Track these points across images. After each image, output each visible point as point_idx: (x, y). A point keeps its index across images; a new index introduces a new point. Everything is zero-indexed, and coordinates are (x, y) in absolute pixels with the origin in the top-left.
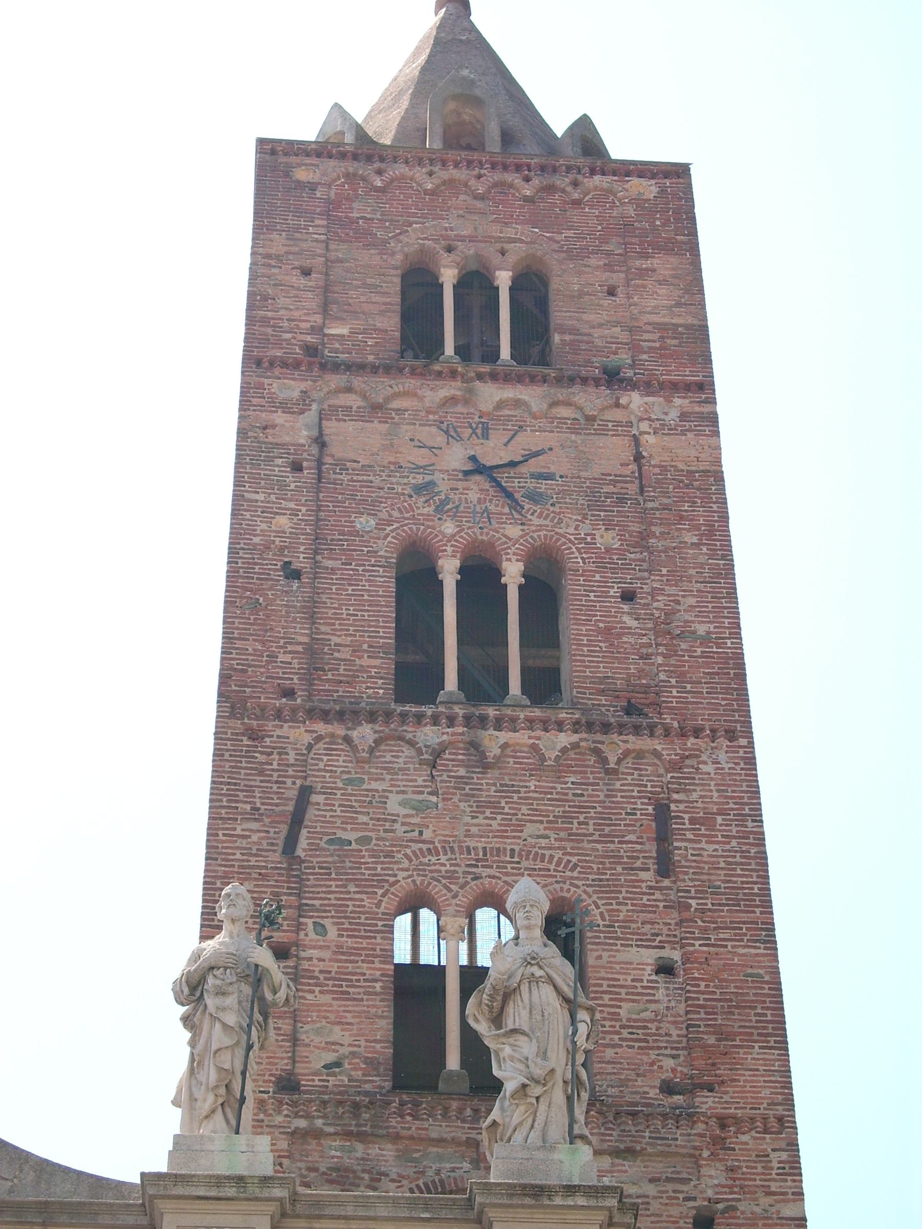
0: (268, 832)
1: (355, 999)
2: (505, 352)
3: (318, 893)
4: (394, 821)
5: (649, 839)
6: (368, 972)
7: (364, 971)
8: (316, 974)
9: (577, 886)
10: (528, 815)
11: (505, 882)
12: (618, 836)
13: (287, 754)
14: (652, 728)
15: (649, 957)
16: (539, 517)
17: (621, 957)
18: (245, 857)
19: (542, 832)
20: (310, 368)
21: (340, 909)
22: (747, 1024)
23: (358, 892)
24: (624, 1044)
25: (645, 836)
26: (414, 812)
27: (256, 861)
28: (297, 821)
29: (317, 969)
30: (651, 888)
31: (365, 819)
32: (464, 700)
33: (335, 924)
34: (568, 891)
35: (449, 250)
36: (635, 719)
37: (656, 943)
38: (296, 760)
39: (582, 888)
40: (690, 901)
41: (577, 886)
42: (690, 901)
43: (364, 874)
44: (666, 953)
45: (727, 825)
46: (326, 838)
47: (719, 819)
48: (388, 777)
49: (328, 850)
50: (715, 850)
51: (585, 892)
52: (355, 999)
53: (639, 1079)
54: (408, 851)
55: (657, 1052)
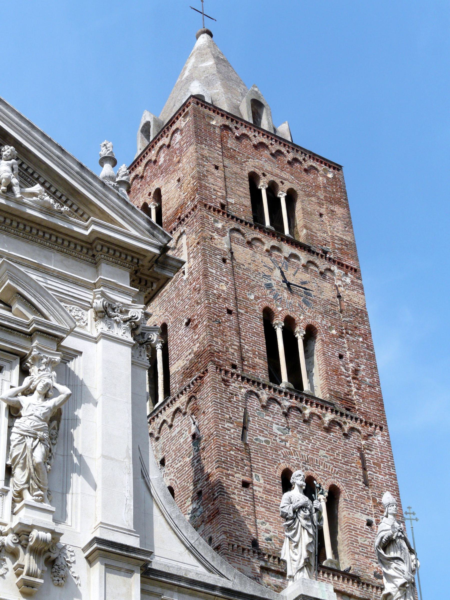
0: (236, 430)
2: (268, 223)
4: (276, 436)
5: (360, 467)
6: (275, 501)
7: (274, 500)
8: (259, 498)
12: (350, 463)
13: (238, 396)
15: (365, 518)
16: (308, 312)
18: (230, 439)
19: (325, 455)
20: (255, 228)
23: (268, 465)
24: (361, 553)
25: (358, 465)
28: (245, 428)
29: (259, 496)
32: (293, 388)
33: (263, 477)
35: (264, 175)
36: (348, 413)
37: (366, 513)
38: (242, 399)
41: (339, 481)
43: (269, 457)
44: (370, 518)
48: (272, 416)
49: (255, 443)
50: (382, 478)
53: (368, 570)
54: (283, 451)
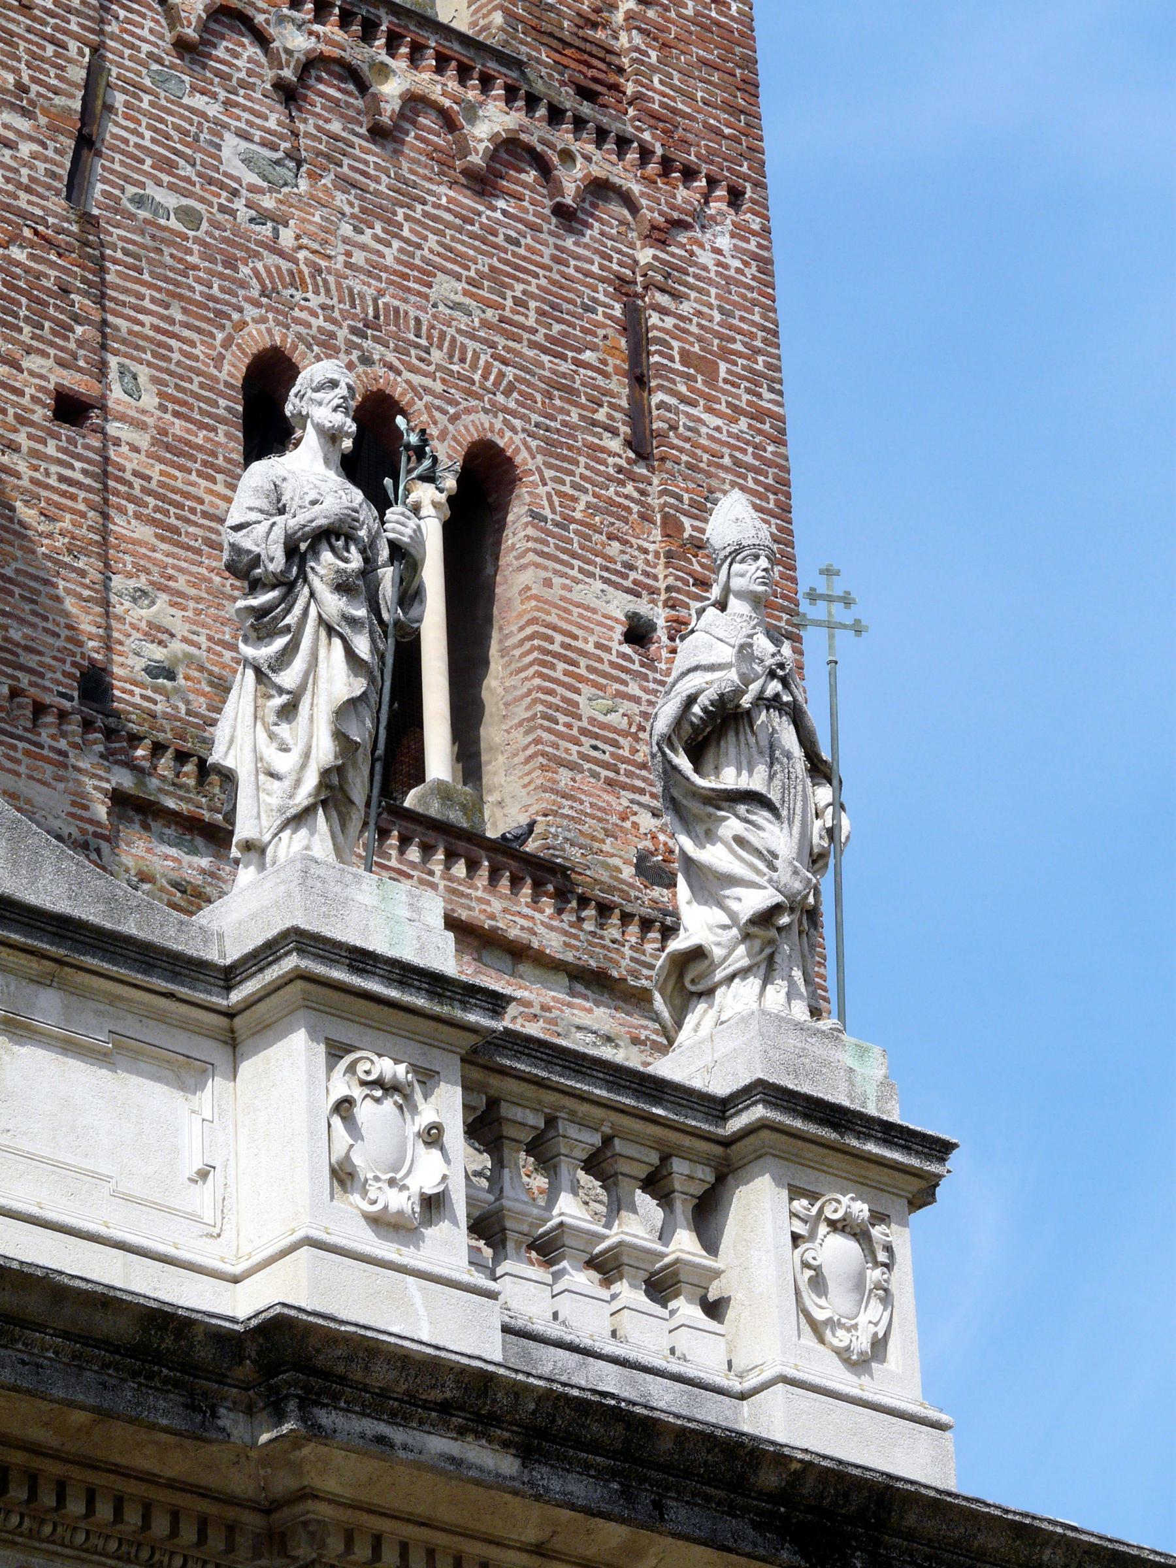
1: (188, 548)
3: (124, 304)
6: (207, 498)
8: (128, 476)
9: (513, 430)
10: (439, 254)
11: (408, 382)
14: (623, 143)
15: (619, 605)
17: (579, 593)
19: (459, 298)
21: (161, 352)
22: (56, 497)
23: (187, 326)
25: (611, 361)
26: (265, 184)
27: (29, 202)
29: (129, 466)
30: (620, 470)
31: (188, 171)
34: (501, 433)
37: (628, 583)
39: (522, 436)
40: (683, 519)
41: (513, 430)
42: (683, 519)
44: (643, 607)
45: (733, 384)
46: (131, 190)
47: (723, 367)
48: (222, 95)
49: (132, 217)
50: (718, 429)
51: (525, 443)
52: (188, 548)
53: (609, 840)
54: (260, 266)
55: (631, 796)
